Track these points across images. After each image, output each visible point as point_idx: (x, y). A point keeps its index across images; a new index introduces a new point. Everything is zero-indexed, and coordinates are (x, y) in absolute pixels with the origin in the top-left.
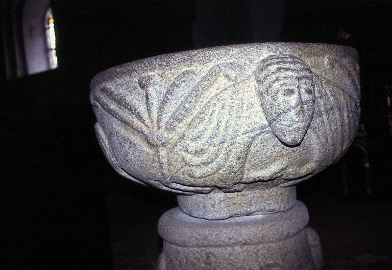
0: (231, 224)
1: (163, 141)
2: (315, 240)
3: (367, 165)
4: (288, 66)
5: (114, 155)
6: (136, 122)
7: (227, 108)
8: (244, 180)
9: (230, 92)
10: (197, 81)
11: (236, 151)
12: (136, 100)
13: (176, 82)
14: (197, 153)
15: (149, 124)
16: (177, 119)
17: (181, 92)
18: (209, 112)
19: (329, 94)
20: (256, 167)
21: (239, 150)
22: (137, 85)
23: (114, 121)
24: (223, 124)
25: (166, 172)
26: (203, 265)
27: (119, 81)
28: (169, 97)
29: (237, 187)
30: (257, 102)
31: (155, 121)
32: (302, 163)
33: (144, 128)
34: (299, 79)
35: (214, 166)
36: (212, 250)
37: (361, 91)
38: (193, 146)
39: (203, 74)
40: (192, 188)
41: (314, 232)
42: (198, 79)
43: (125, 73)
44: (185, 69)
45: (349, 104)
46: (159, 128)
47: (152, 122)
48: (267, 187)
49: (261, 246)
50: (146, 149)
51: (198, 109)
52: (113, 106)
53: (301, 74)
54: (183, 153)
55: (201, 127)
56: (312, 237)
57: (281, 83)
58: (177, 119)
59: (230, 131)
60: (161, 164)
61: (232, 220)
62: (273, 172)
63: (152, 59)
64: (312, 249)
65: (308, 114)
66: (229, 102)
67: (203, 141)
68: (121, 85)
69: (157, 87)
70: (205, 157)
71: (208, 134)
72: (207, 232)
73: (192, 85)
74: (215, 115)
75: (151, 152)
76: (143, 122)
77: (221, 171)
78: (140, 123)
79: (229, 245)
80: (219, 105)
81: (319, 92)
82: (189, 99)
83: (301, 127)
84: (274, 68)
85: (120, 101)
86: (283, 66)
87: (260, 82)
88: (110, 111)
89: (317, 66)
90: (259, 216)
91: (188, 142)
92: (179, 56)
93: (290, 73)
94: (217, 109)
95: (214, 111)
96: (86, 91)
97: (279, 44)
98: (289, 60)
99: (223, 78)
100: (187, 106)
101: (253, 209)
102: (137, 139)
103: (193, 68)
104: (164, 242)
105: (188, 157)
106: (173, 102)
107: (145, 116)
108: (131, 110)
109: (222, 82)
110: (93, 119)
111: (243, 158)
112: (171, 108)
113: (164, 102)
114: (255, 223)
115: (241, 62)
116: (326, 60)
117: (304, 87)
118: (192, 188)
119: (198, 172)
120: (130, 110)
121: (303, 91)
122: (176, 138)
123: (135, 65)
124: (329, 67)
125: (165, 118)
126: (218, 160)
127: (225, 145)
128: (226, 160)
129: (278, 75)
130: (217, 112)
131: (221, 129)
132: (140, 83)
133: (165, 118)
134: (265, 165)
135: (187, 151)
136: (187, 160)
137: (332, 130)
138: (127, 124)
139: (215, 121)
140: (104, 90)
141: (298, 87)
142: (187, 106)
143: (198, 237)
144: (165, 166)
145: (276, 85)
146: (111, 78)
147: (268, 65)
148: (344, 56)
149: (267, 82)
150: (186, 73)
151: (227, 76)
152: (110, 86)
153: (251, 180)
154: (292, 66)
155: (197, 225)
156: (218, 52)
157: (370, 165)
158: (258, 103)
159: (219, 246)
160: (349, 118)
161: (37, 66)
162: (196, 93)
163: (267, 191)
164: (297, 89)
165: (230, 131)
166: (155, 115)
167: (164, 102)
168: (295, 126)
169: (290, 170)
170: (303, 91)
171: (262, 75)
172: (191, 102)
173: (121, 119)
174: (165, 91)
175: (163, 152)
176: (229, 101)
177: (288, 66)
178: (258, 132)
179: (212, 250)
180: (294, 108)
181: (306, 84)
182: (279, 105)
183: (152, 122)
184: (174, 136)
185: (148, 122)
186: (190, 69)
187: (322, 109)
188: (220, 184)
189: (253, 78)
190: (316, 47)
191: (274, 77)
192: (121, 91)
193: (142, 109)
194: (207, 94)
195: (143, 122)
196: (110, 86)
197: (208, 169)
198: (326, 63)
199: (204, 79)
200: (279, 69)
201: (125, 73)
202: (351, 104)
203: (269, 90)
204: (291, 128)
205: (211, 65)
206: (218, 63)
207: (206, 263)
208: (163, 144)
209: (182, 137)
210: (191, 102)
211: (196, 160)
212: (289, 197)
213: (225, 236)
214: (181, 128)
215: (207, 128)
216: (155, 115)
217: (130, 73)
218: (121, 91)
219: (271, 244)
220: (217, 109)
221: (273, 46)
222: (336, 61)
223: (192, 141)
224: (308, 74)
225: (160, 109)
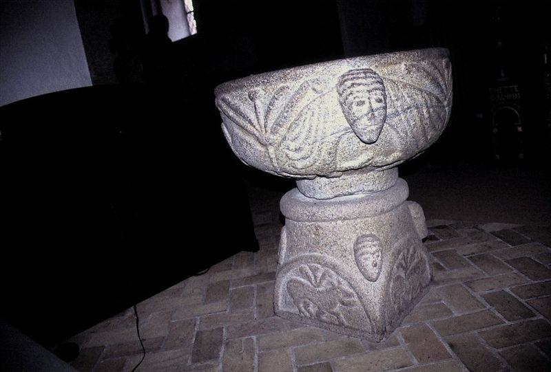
0: (334, 203)
1: (270, 141)
2: (417, 213)
3: (520, 129)
4: (360, 81)
5: (237, 151)
6: (250, 127)
7: (316, 115)
8: (338, 169)
9: (317, 102)
10: (292, 94)
11: (325, 148)
12: (246, 109)
13: (276, 96)
14: (297, 150)
15: (259, 129)
16: (278, 124)
17: (281, 103)
18: (303, 119)
19: (406, 96)
20: (346, 159)
21: (329, 147)
22: (247, 97)
23: (234, 124)
24: (314, 128)
25: (276, 165)
26: (313, 236)
27: (234, 93)
28: (271, 107)
29: (335, 174)
30: (339, 109)
31: (263, 126)
32: (387, 154)
33: (256, 132)
34: (369, 91)
35: (311, 160)
36: (320, 224)
37: (267, 173)
38: (293, 145)
39: (296, 89)
40: (299, 176)
41: (418, 205)
42: (292, 93)
43: (237, 87)
44: (282, 85)
45: (429, 102)
46: (266, 132)
47: (261, 127)
48: (364, 172)
49: (359, 220)
50: (259, 147)
51: (294, 117)
52: (231, 114)
53: (372, 87)
54: (286, 151)
55: (297, 131)
56: (416, 211)
57: (354, 96)
58: (278, 124)
59: (320, 133)
60: (271, 159)
61: (338, 199)
62: (360, 162)
63: (256, 77)
64: (416, 222)
65: (379, 118)
66: (317, 111)
67: (301, 141)
68: (236, 97)
69: (262, 99)
70: (303, 154)
71: (303, 136)
72: (315, 209)
73: (289, 98)
74: (307, 121)
75: (263, 149)
76: (254, 127)
77: (317, 164)
78: (252, 127)
79: (332, 220)
80: (310, 113)
81: (395, 96)
82: (287, 109)
83: (374, 129)
84: (349, 83)
85: (236, 110)
86: (357, 81)
87: (340, 95)
88: (229, 117)
89: (394, 73)
90: (360, 196)
91: (289, 142)
92: (277, 74)
93: (361, 88)
94: (308, 116)
95: (306, 118)
96: (213, 97)
97: (358, 59)
98: (363, 75)
99: (312, 90)
100: (285, 114)
101: (353, 190)
102: (252, 140)
103: (288, 84)
104: (286, 219)
105: (291, 154)
106: (275, 111)
107: (255, 122)
108: (245, 117)
109: (310, 94)
110: (221, 121)
111: (333, 153)
112: (273, 116)
113: (268, 112)
114: (361, 201)
115: (325, 78)
116: (403, 66)
117: (375, 97)
118: (299, 176)
119: (300, 165)
120: (244, 117)
121: (373, 101)
122: (280, 139)
123: (244, 81)
124: (406, 72)
125: (270, 124)
126: (313, 155)
127: (318, 144)
128: (319, 155)
129: (352, 89)
130: (308, 119)
131: (313, 132)
132: (249, 97)
133: (270, 124)
134: (353, 157)
135: (288, 149)
136: (290, 156)
137: (410, 126)
138: (242, 128)
139: (308, 126)
140: (224, 100)
141: (369, 98)
142: (285, 114)
143: (308, 214)
144: (274, 161)
145: (351, 98)
146: (228, 91)
147: (345, 80)
148: (423, 60)
149: (344, 95)
150: (282, 89)
151: (314, 89)
152: (228, 97)
153: (343, 169)
154: (364, 81)
155: (307, 203)
156: (306, 70)
157: (517, 129)
158: (341, 110)
159: (324, 221)
160: (429, 113)
161: (178, 33)
162: (291, 105)
163: (365, 175)
164: (367, 101)
165: (320, 133)
166: (262, 122)
167: (268, 112)
168: (369, 129)
169: (377, 159)
170: (373, 101)
171: (341, 90)
172: (288, 111)
173: (237, 124)
174: (268, 103)
175: (271, 150)
176: (318, 110)
177: (360, 81)
178: (343, 132)
179: (320, 224)
180: (366, 115)
181: (376, 94)
182: (354, 114)
183: (261, 127)
184: (276, 138)
185: (257, 127)
186: (285, 85)
187: (400, 110)
188: (319, 173)
189: (335, 90)
190: (392, 57)
191: (349, 91)
192: (236, 101)
193: (252, 116)
194: (300, 104)
195: (254, 127)
196: (228, 97)
197: (307, 162)
198: (403, 69)
199: (297, 93)
200: (353, 84)
201: (237, 87)
202: (431, 100)
203: (346, 101)
204: (365, 131)
205: (302, 81)
206: (307, 79)
207: (315, 234)
208: (270, 144)
209: (284, 139)
210: (288, 111)
211: (297, 156)
212: (387, 179)
213: (328, 213)
214: (283, 131)
215: (301, 130)
216: (262, 122)
217: (241, 87)
218: (236, 101)
219: (367, 219)
220: (308, 116)
221: (352, 61)
222: (413, 66)
223: (292, 141)
224: (378, 86)
225: (266, 117)
